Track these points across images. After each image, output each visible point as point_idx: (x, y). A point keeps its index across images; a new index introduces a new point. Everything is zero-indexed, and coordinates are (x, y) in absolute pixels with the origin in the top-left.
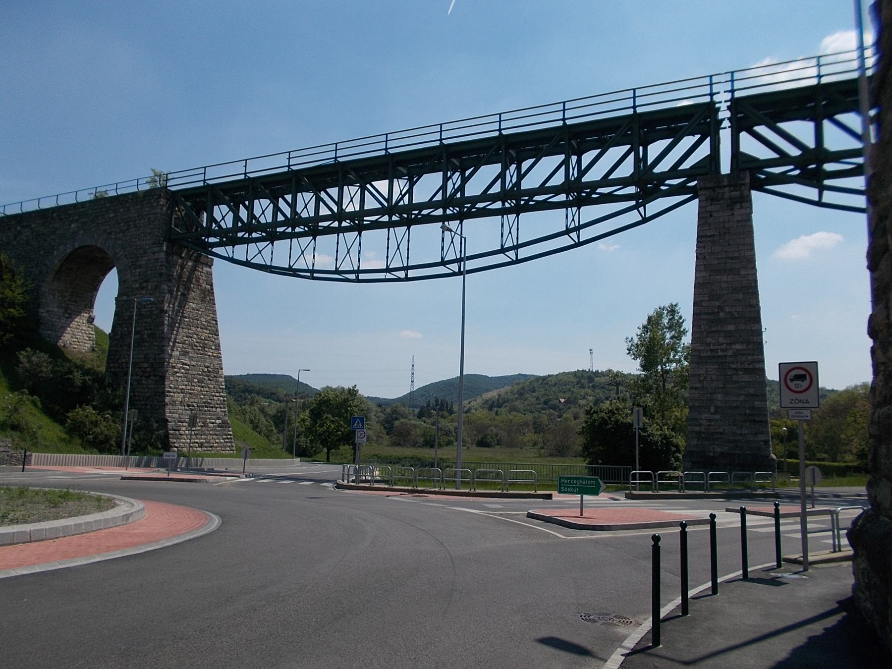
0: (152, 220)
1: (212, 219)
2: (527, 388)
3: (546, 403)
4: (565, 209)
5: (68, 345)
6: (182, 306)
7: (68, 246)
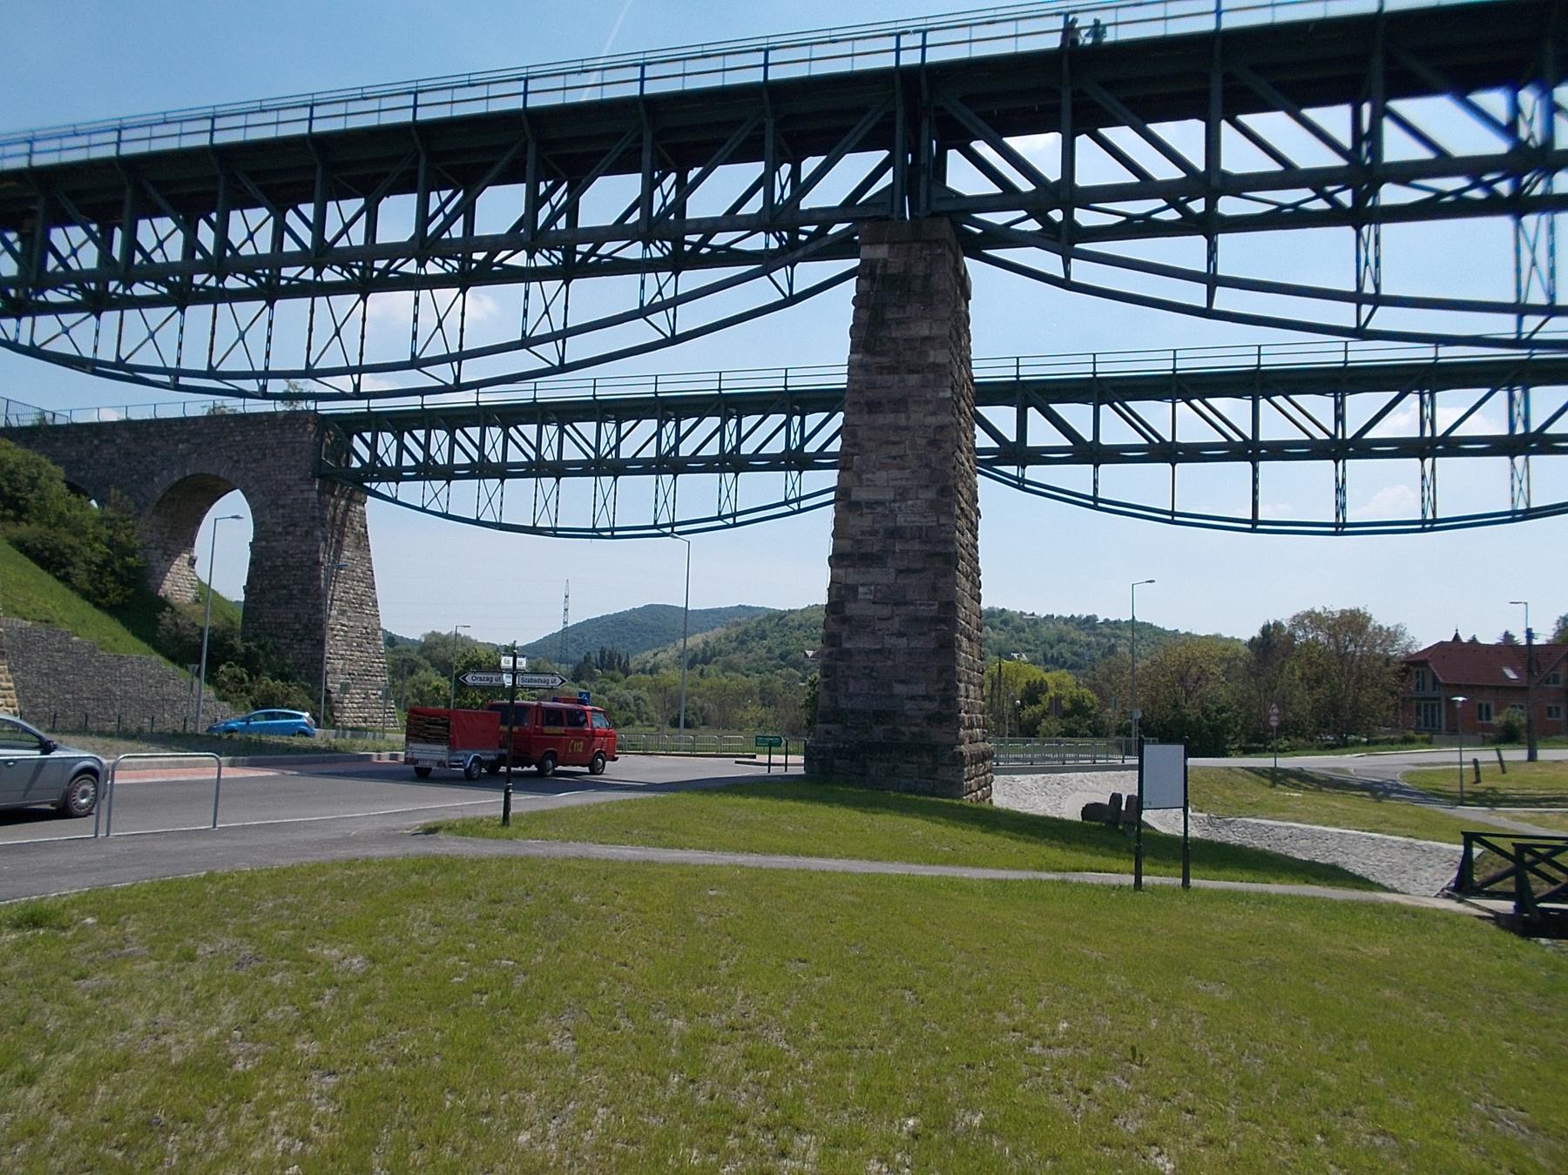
0: (298, 450)
2: (752, 633)
3: (783, 657)
5: (170, 596)
6: (337, 555)
7: (175, 472)
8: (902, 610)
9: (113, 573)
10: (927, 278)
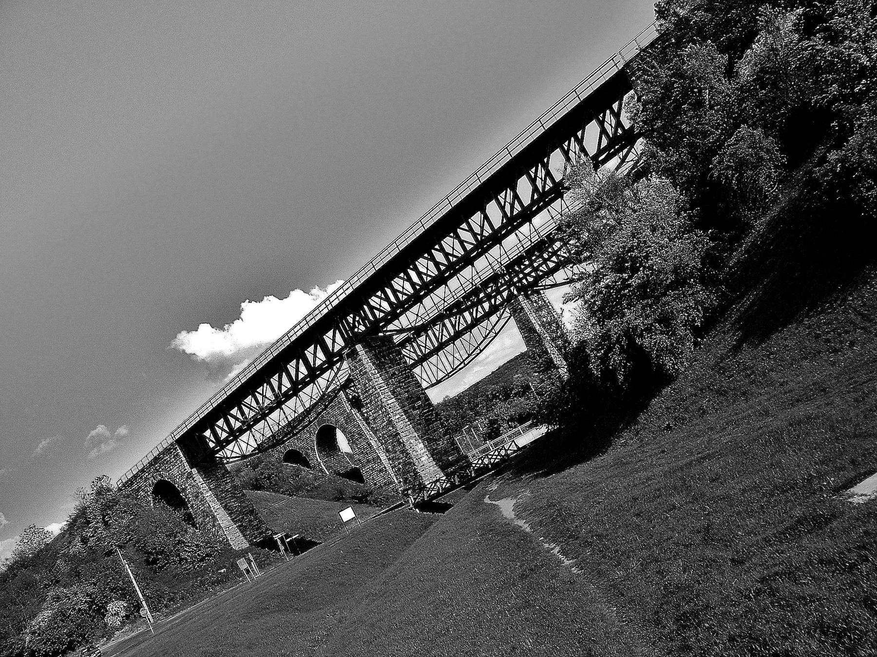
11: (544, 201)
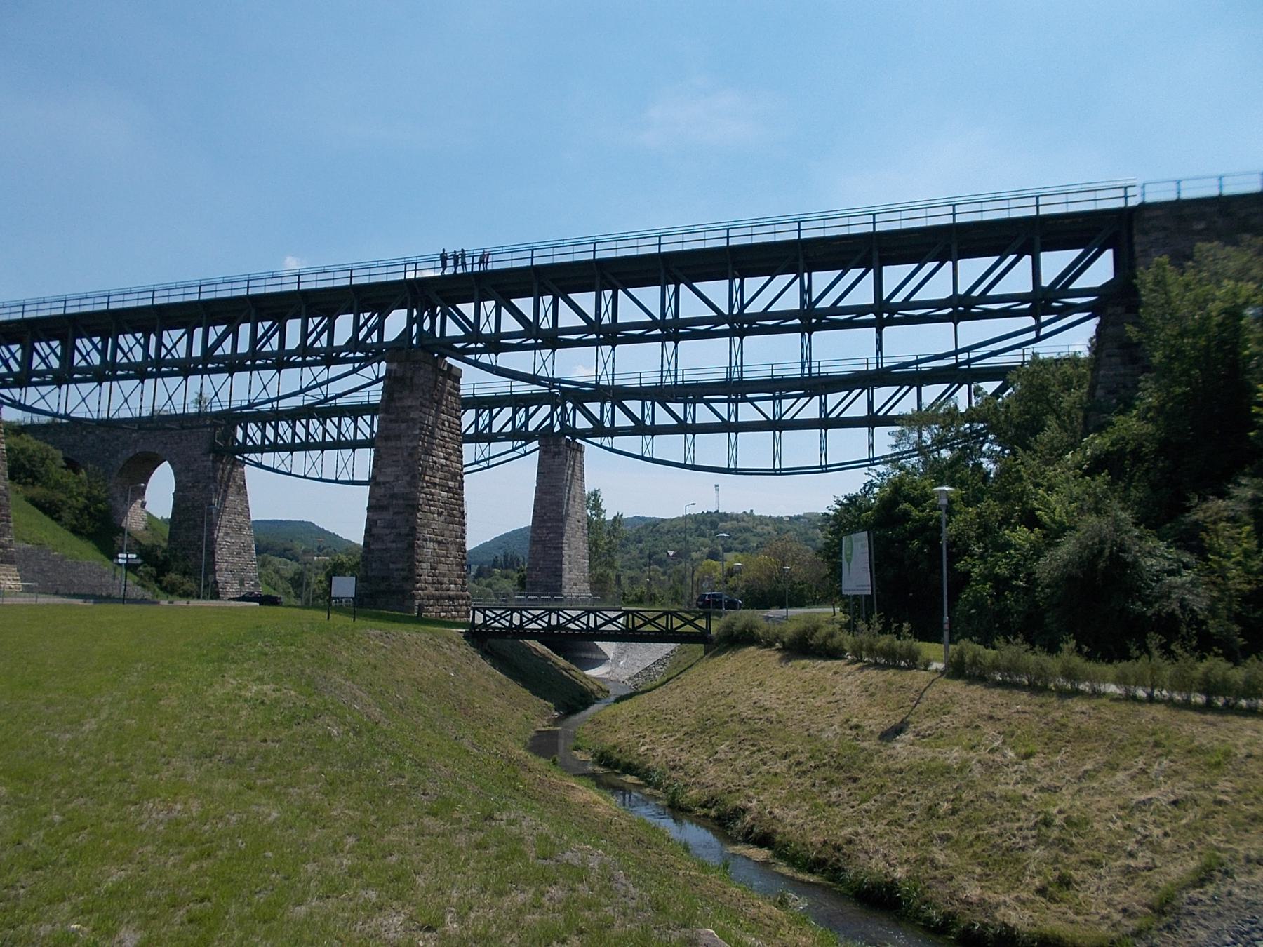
1: (246, 435)
2: (632, 538)
4: (610, 347)
6: (224, 500)
8: (394, 531)
9: (89, 513)
10: (412, 378)
11: (253, 362)
